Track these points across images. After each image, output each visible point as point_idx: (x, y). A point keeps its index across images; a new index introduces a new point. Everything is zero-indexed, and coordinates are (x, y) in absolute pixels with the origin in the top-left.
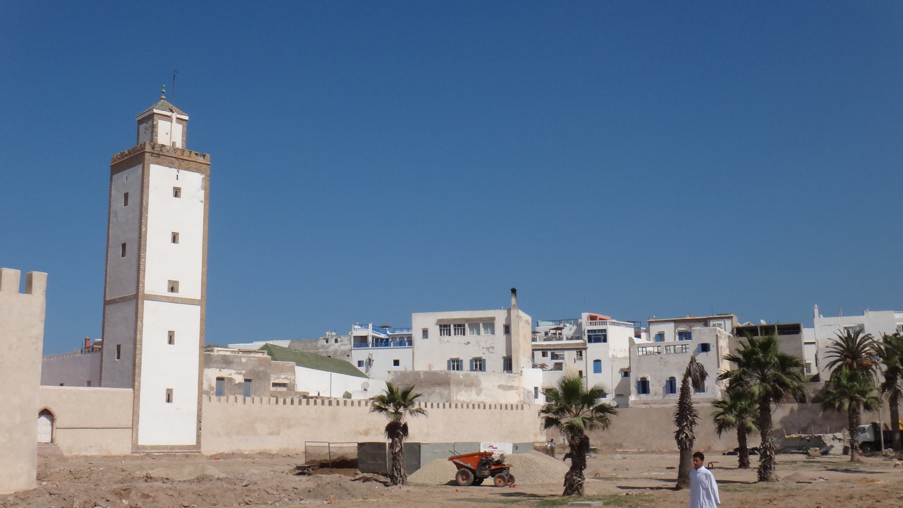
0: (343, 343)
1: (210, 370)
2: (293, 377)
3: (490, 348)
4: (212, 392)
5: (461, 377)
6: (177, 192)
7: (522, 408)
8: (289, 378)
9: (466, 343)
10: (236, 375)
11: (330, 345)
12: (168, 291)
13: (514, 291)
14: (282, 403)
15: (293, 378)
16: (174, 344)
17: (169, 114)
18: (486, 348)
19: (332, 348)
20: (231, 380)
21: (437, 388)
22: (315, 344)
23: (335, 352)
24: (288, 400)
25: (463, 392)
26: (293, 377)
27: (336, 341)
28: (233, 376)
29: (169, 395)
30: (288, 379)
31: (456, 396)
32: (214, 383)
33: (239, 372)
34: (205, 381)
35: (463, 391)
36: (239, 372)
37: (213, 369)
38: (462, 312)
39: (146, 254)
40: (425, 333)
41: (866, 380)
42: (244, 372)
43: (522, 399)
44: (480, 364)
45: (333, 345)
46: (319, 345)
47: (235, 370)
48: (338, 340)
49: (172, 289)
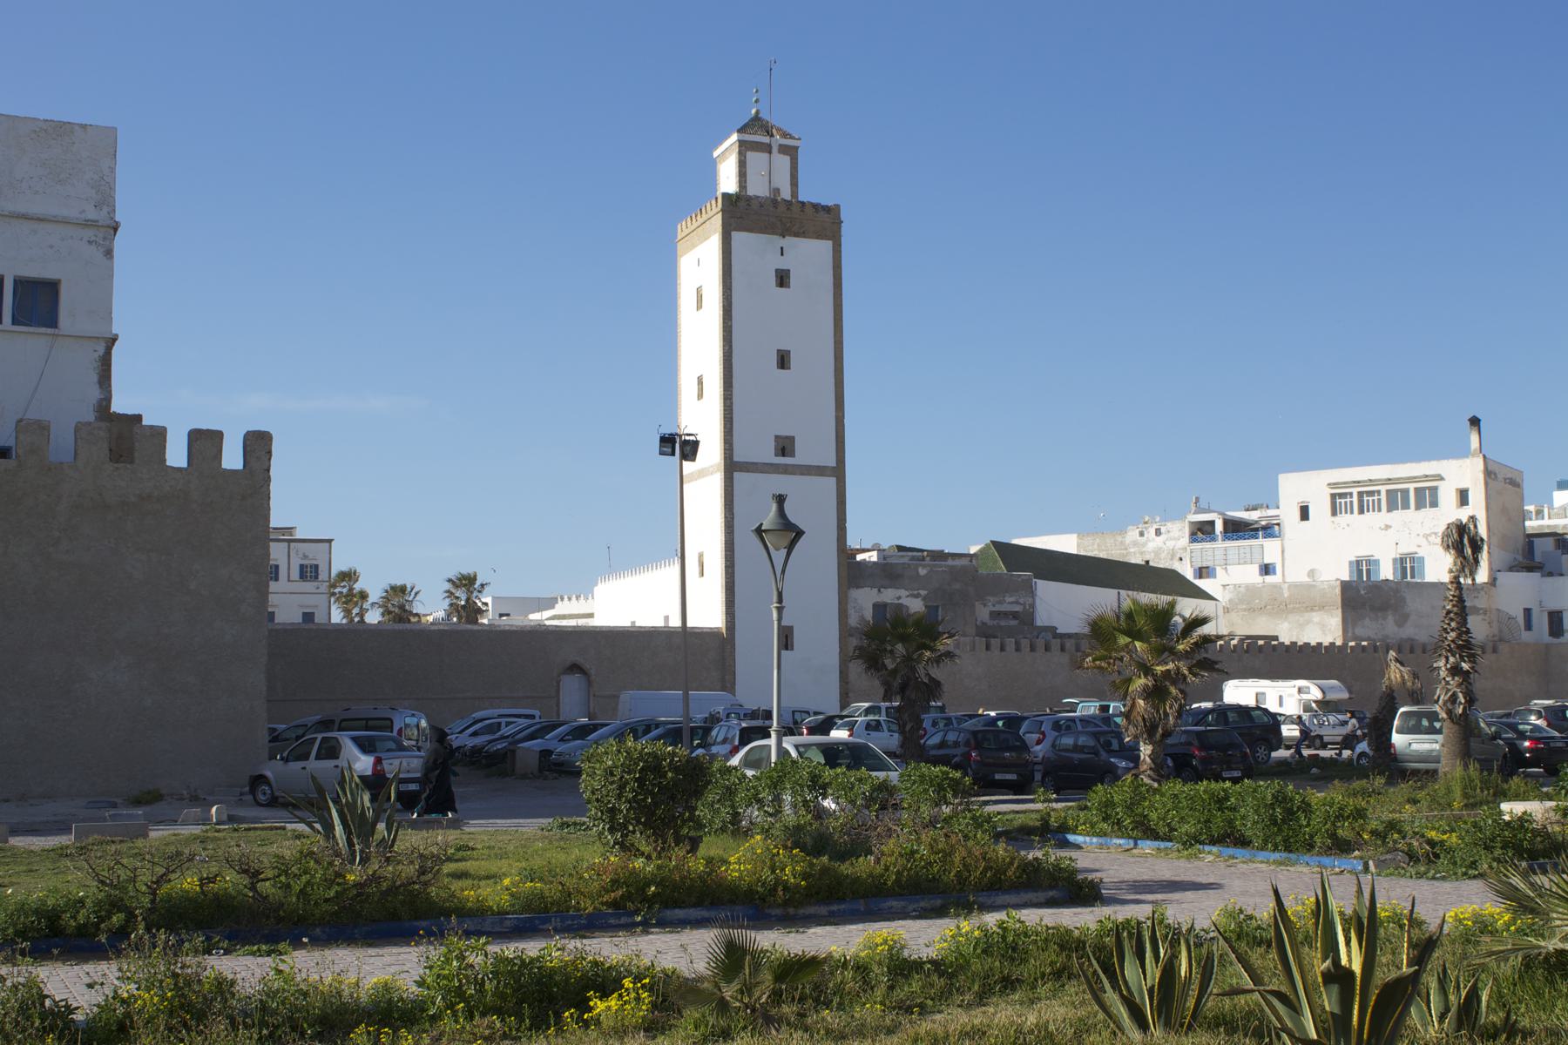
0: (1171, 534)
1: (861, 591)
3: (1429, 535)
5: (1362, 592)
6: (783, 279)
7: (1495, 650)
8: (1021, 601)
9: (1383, 527)
10: (909, 599)
11: (1148, 540)
12: (776, 455)
13: (1475, 422)
14: (1029, 649)
17: (766, 139)
18: (1424, 536)
19: (1151, 546)
21: (1314, 614)
22: (1119, 539)
23: (1158, 552)
24: (1025, 643)
25: (1367, 621)
27: (1158, 532)
28: (905, 601)
29: (787, 637)
31: (1353, 629)
33: (916, 592)
34: (851, 612)
35: (1367, 619)
36: (916, 592)
38: (1408, 466)
40: (1304, 513)
42: (923, 593)
43: (1496, 632)
44: (1411, 567)
45: (1153, 539)
46: (1127, 542)
47: (906, 590)
48: (1162, 531)
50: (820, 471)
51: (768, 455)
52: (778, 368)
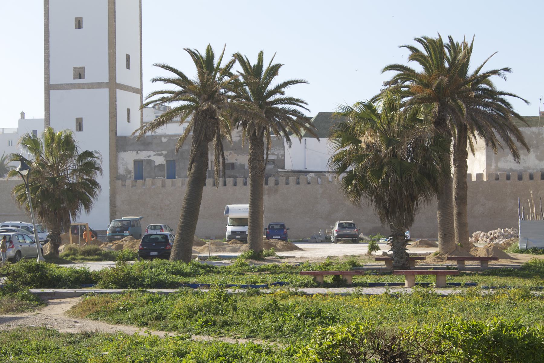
1: (126, 153)
2: (282, 152)
4: (129, 176)
10: (156, 157)
15: (282, 153)
16: (82, 131)
20: (150, 162)
26: (282, 152)
28: (152, 158)
30: (276, 155)
32: (131, 167)
33: (160, 153)
36: (160, 153)
37: (130, 153)
39: (49, 45)
41: (314, 319)
42: (164, 152)
47: (154, 151)
49: (80, 77)
50: (99, 85)
51: (69, 79)
52: (76, 28)
